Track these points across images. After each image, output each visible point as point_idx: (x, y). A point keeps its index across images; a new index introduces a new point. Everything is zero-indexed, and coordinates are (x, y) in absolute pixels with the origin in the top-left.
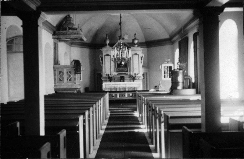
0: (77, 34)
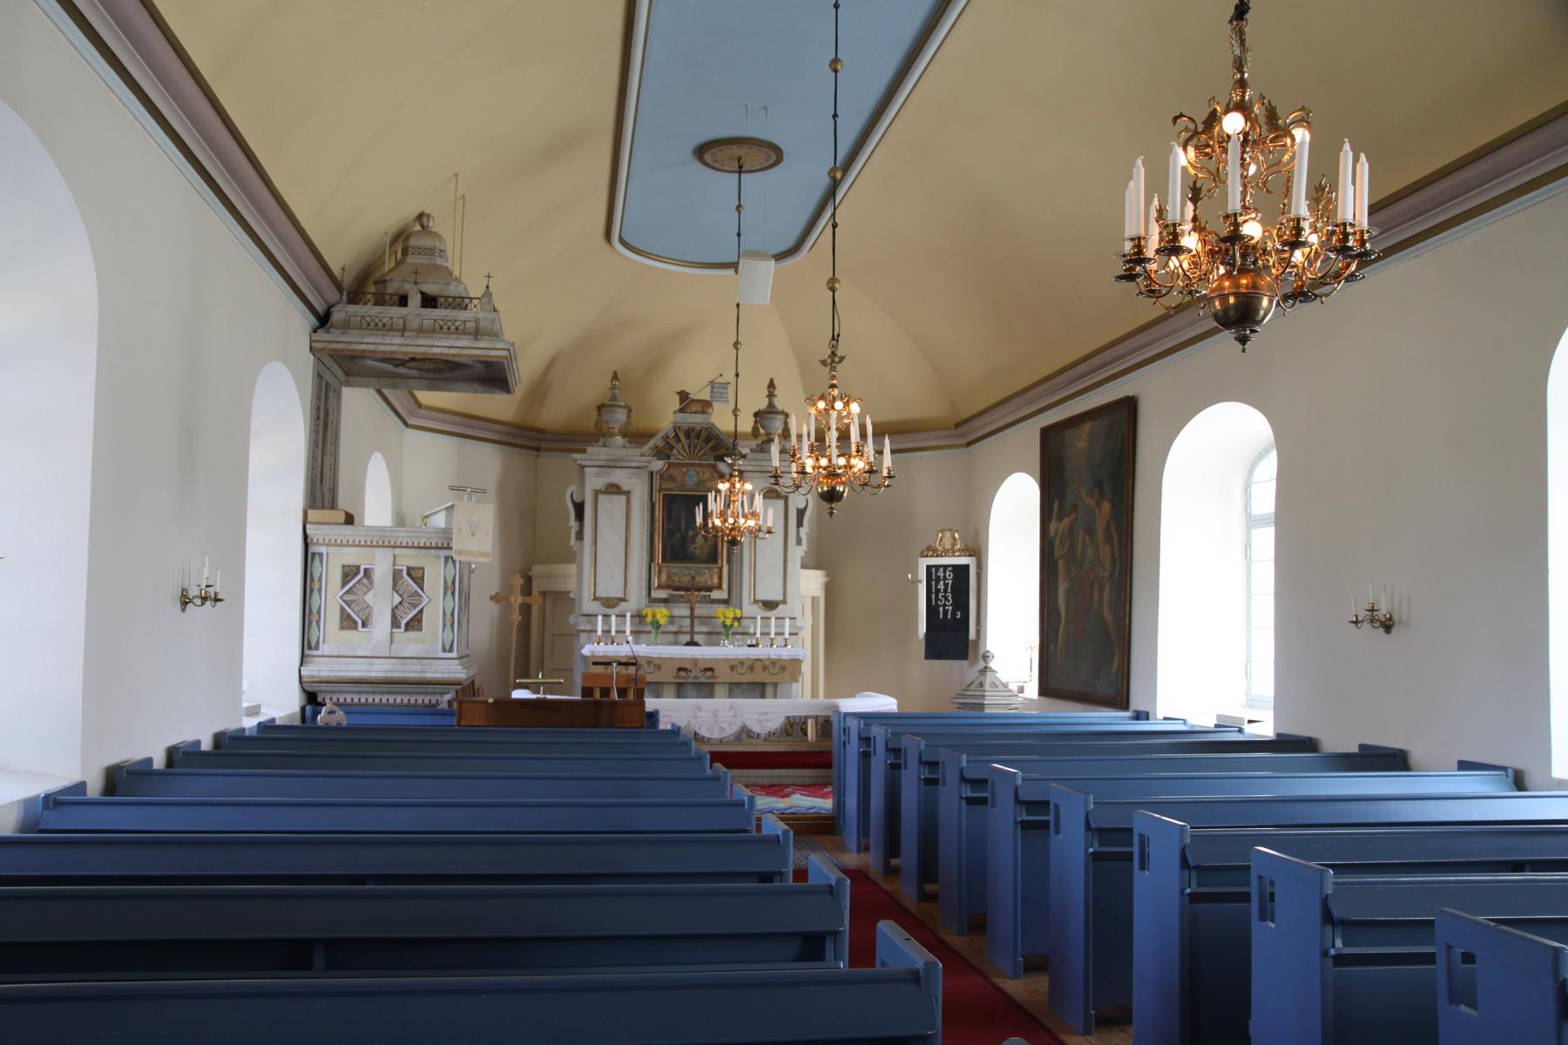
0: (477, 333)
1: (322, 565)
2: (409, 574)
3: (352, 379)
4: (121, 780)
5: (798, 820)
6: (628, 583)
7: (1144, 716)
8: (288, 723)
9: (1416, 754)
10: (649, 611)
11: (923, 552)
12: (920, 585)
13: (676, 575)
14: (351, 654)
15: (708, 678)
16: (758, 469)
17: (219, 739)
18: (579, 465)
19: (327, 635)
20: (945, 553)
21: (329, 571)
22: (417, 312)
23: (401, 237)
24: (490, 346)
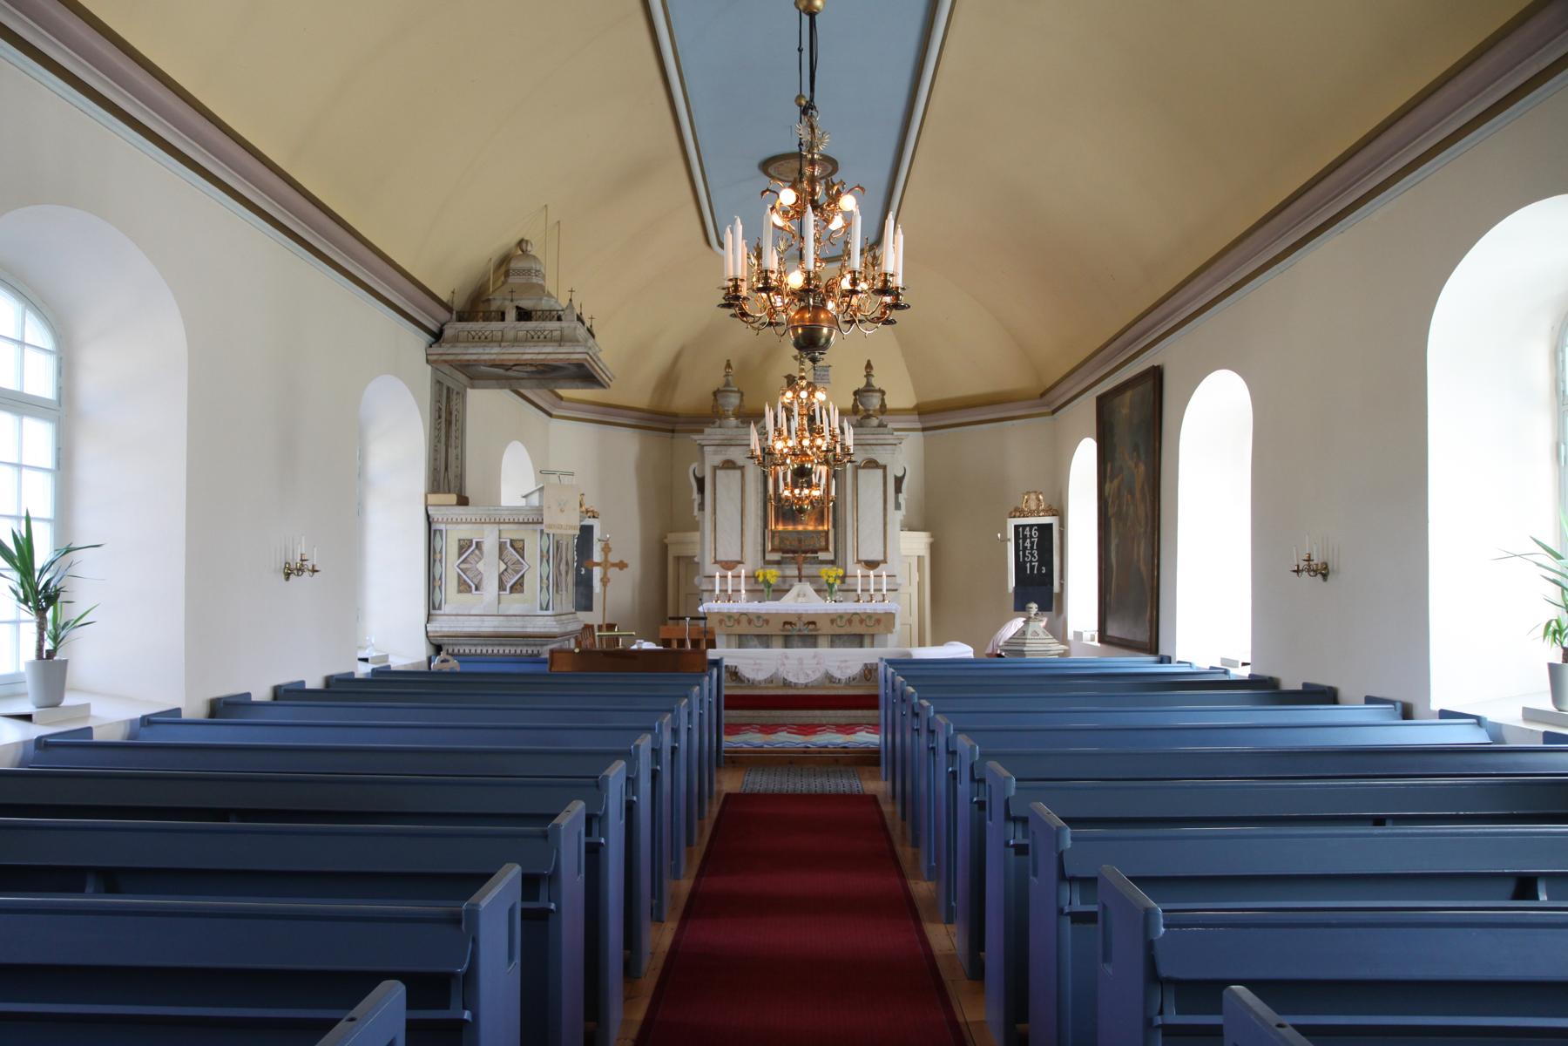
0: (561, 340)
2: (512, 546)
3: (476, 382)
4: (221, 709)
5: (847, 753)
6: (745, 548)
7: (1165, 660)
8: (412, 669)
9: (1344, 693)
10: (760, 572)
11: (1011, 513)
12: (1009, 543)
13: (787, 539)
14: (466, 613)
15: (811, 630)
17: (329, 680)
18: (699, 444)
19: (448, 597)
20: (1031, 513)
21: (448, 544)
22: (512, 325)
24: (572, 351)
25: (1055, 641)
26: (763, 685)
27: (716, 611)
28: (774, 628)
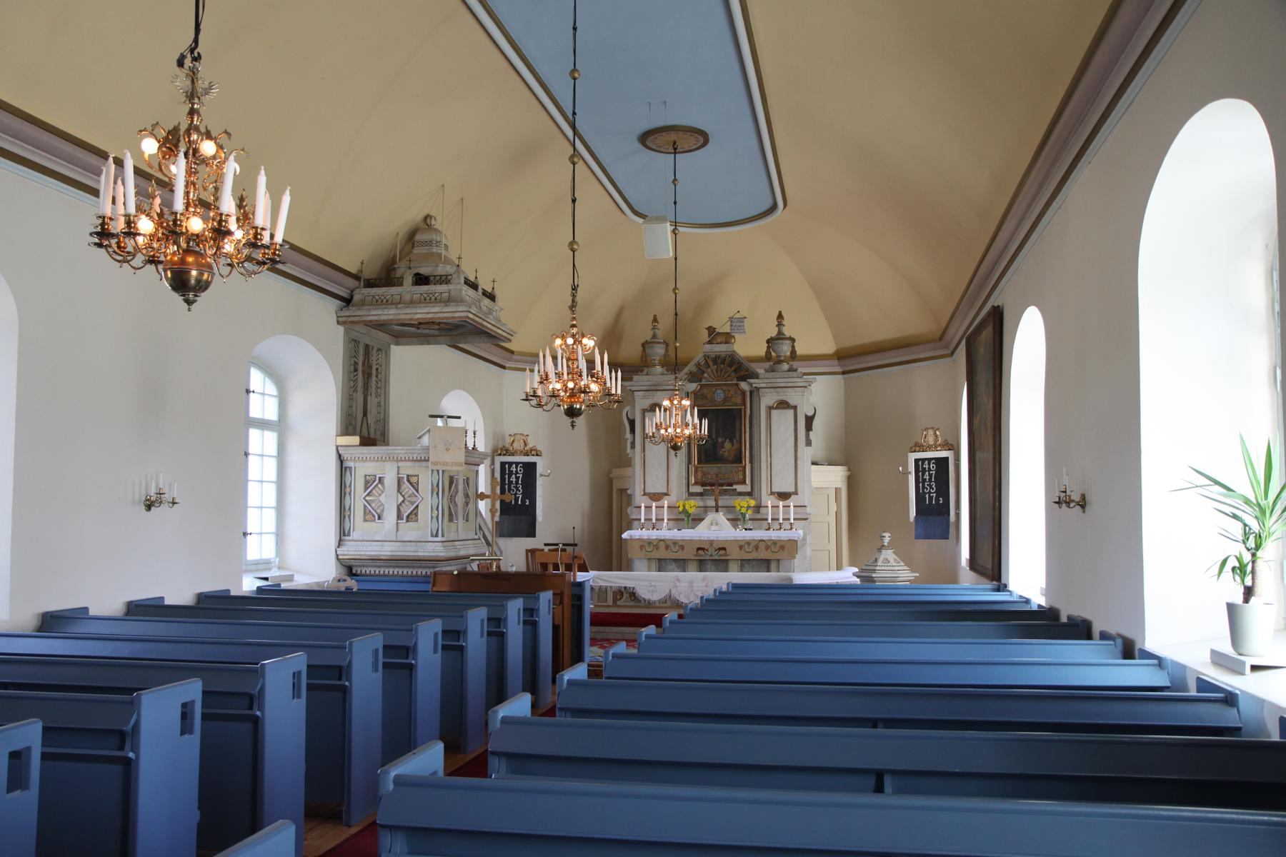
0: (449, 301)
1: (351, 476)
2: (408, 481)
3: (400, 339)
4: (51, 623)
6: (670, 481)
8: (316, 588)
11: (912, 447)
15: (721, 555)
16: (769, 385)
17: (202, 598)
20: (929, 448)
21: (356, 479)
22: (408, 290)
23: (411, 237)
24: (455, 310)
25: (906, 568)
26: (658, 605)
27: (637, 537)
28: (689, 553)
